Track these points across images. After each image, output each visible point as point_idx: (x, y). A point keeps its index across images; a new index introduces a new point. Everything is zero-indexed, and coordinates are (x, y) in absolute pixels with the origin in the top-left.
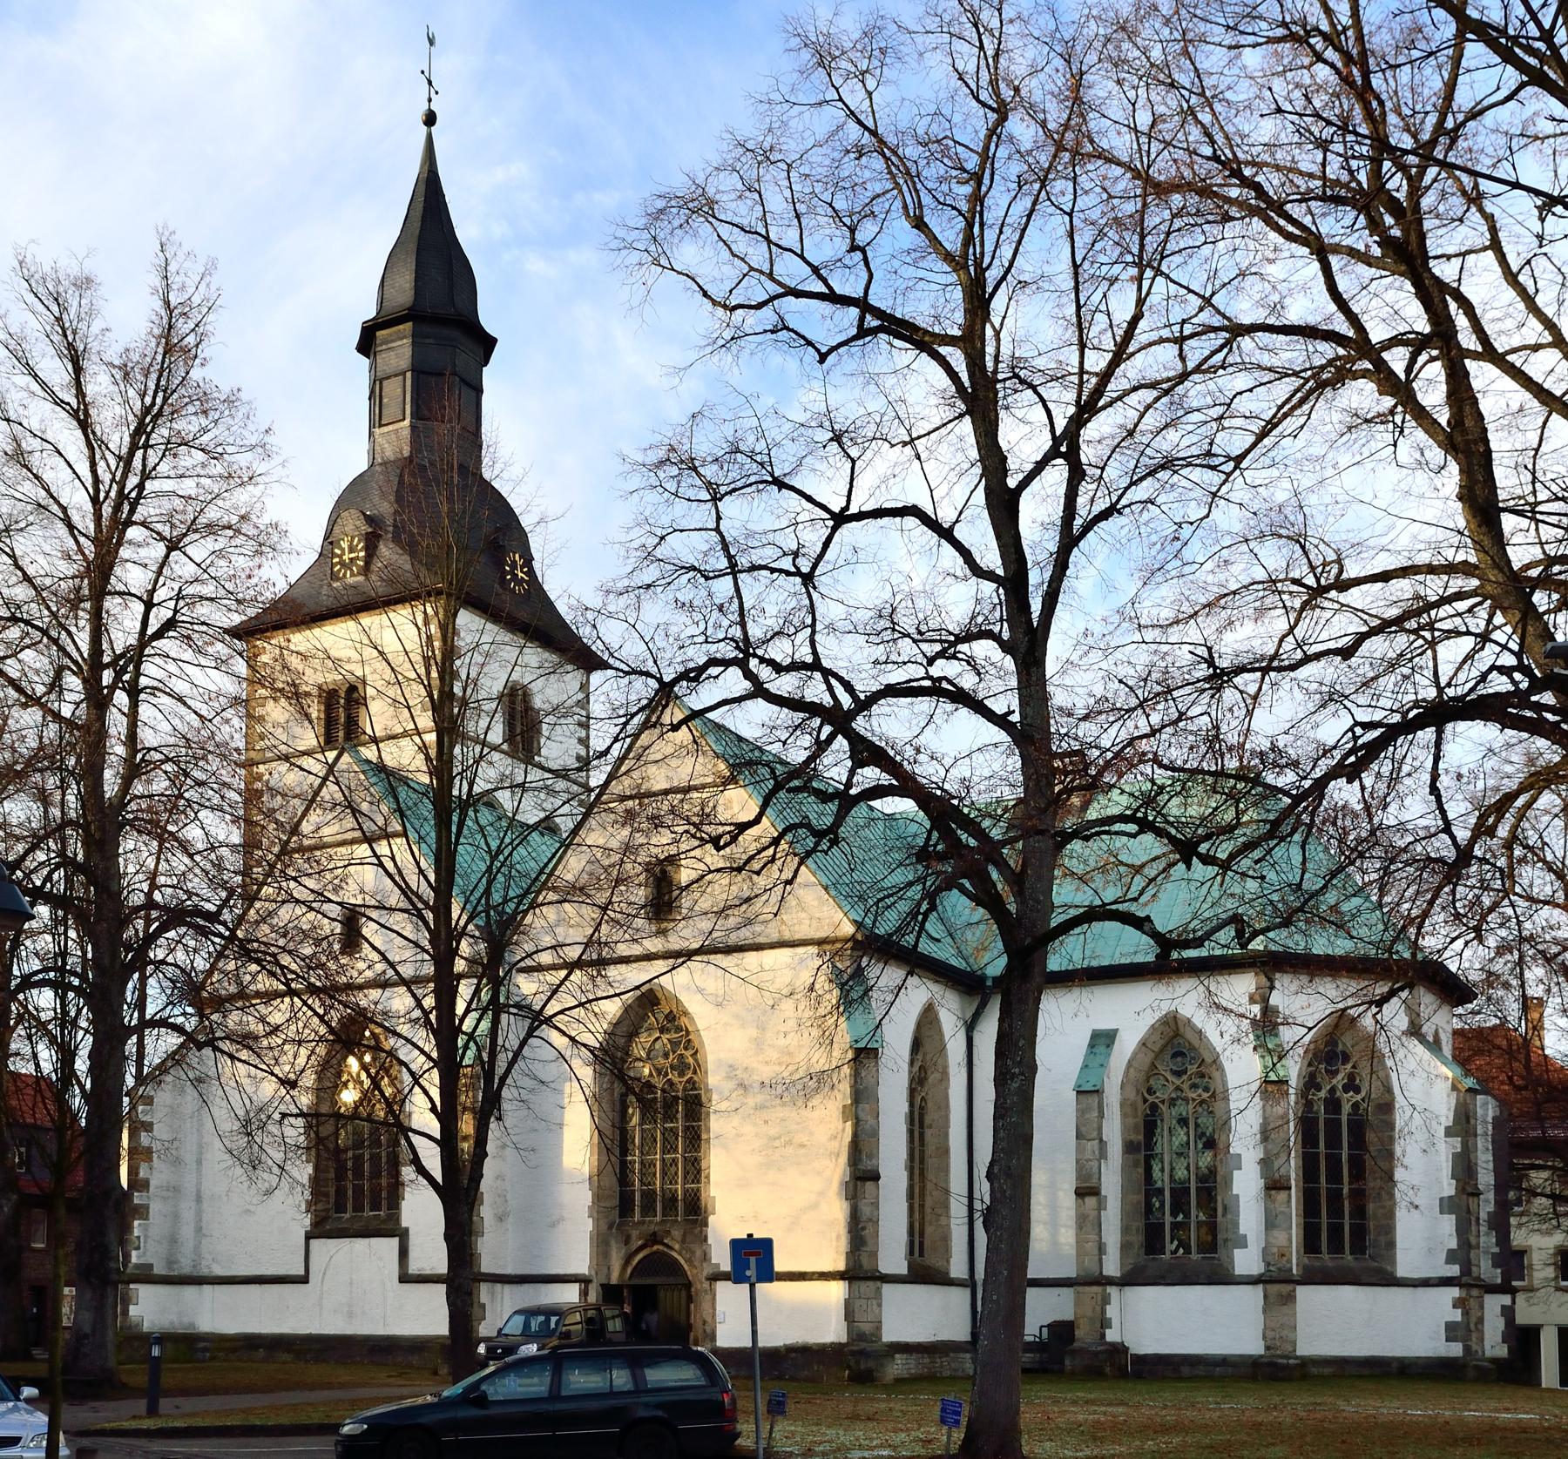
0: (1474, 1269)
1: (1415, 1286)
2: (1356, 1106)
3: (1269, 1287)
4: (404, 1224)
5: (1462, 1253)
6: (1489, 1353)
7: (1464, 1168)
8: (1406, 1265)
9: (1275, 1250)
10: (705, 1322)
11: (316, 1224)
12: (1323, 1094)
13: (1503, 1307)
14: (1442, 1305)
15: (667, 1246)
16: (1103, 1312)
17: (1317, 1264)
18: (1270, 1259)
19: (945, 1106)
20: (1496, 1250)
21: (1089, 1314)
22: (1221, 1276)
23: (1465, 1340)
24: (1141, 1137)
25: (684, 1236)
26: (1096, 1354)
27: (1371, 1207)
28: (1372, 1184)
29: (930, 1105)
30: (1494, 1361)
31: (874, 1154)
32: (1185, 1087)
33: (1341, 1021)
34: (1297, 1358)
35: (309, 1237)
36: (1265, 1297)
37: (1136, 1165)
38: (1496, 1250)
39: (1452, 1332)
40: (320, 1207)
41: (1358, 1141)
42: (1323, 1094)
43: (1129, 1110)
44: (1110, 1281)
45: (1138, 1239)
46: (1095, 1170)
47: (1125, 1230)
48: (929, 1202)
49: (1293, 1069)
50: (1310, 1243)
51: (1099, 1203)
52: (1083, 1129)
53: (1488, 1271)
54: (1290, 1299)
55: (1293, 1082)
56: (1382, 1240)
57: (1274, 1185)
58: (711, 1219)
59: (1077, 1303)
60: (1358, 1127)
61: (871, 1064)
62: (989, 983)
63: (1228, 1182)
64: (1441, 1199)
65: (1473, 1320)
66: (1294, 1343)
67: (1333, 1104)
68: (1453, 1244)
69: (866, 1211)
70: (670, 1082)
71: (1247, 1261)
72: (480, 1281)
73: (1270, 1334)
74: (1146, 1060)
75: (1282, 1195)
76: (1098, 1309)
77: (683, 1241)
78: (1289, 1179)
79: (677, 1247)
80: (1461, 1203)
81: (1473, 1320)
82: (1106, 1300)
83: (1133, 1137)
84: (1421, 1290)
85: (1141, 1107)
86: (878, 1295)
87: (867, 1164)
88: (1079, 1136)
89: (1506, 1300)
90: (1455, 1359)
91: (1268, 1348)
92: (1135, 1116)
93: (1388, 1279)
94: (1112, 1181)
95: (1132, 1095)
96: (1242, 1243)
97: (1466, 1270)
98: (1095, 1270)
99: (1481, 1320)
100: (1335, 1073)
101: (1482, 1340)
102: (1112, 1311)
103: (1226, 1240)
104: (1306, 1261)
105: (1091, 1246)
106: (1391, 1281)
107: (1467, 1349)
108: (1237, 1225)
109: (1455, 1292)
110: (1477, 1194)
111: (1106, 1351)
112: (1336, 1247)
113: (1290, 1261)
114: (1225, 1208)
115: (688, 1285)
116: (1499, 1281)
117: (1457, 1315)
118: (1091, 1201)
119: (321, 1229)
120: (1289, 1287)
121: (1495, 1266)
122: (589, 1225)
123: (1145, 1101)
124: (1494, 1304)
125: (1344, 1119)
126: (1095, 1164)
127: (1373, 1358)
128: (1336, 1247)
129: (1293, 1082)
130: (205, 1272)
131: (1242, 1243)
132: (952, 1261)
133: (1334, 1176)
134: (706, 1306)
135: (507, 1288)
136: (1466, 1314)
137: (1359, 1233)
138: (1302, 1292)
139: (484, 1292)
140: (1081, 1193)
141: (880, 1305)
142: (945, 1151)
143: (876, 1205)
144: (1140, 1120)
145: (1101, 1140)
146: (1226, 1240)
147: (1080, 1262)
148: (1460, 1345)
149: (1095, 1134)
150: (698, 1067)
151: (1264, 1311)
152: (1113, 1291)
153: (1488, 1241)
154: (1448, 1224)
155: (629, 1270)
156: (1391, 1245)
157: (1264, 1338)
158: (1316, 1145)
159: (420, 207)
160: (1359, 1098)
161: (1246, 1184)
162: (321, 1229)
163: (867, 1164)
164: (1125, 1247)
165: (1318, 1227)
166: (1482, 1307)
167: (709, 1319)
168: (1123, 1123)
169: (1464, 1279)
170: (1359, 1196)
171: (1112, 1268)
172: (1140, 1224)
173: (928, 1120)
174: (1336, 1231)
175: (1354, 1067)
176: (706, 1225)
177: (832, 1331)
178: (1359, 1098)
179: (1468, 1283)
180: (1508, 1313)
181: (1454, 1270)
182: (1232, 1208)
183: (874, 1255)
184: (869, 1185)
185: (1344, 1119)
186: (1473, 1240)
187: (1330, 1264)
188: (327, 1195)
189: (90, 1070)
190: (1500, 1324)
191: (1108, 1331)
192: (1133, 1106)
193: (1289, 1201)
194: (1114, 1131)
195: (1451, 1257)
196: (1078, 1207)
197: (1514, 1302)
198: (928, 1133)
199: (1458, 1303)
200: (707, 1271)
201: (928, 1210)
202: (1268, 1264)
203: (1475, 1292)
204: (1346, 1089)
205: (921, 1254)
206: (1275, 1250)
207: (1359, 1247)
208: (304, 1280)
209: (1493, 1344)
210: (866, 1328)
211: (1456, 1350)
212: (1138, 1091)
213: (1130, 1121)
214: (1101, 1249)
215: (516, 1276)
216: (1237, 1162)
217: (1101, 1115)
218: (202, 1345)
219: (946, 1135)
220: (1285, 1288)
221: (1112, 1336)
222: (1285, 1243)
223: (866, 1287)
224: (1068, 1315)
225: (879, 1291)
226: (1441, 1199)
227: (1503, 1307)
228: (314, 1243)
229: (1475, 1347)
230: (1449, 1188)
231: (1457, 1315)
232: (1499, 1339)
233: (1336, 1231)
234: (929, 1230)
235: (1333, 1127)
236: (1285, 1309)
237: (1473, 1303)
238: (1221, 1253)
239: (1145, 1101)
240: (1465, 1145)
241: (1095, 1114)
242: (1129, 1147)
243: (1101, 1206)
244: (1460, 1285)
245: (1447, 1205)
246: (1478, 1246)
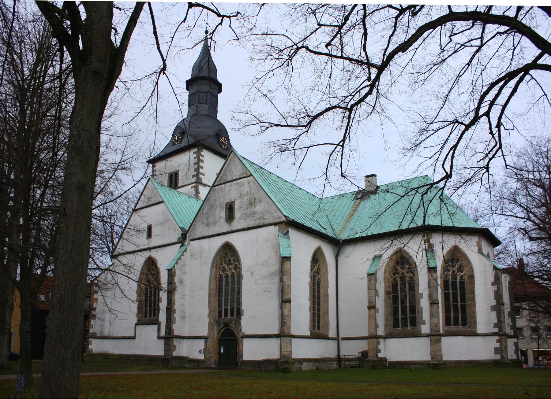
0: (503, 329)
1: (484, 336)
2: (462, 277)
3: (432, 337)
4: (160, 321)
5: (499, 324)
6: (510, 358)
7: (498, 296)
8: (481, 329)
9: (434, 324)
10: (240, 352)
11: (138, 321)
12: (450, 273)
13: (515, 343)
14: (493, 342)
15: (230, 326)
16: (377, 347)
17: (450, 329)
18: (432, 327)
19: (327, 281)
20: (511, 324)
21: (373, 348)
22: (417, 335)
23: (501, 354)
24: (391, 290)
25: (235, 323)
26: (374, 361)
27: (468, 310)
28: (468, 303)
29: (322, 281)
30: (512, 360)
31: (289, 293)
32: (405, 272)
33: (456, 250)
34: (443, 361)
35: (136, 325)
36: (431, 341)
37: (390, 299)
38: (511, 324)
39: (497, 351)
40: (140, 315)
41: (463, 288)
42: (450, 273)
43: (387, 281)
44: (380, 337)
45: (391, 323)
46: (374, 299)
47: (386, 320)
48: (321, 312)
49: (439, 263)
50: (447, 322)
51: (376, 311)
52: (370, 286)
53: (508, 330)
54: (440, 341)
55: (439, 269)
56: (472, 320)
57: (433, 303)
58: (242, 317)
59: (369, 344)
60: (462, 283)
61: (288, 262)
62: (341, 241)
63: (419, 303)
64: (491, 306)
65: (504, 346)
66: (441, 356)
67: (454, 276)
68: (496, 321)
69: (286, 312)
70: (233, 273)
71: (425, 329)
72: (173, 338)
73: (432, 353)
74: (392, 264)
75: (435, 306)
76: (375, 346)
77: (235, 325)
78: (438, 300)
79: (233, 327)
80: (498, 307)
81: (504, 346)
82: (379, 343)
83: (389, 290)
84: (485, 337)
85: (391, 280)
86: (290, 342)
87: (286, 297)
88: (369, 289)
89: (515, 340)
90: (498, 360)
91: (432, 358)
92: (389, 282)
93: (475, 334)
94: (381, 303)
95: (387, 275)
96: (424, 323)
97: (501, 330)
98: (374, 333)
99: (506, 347)
100: (453, 266)
101: (507, 353)
102: (380, 347)
103: (419, 322)
104: (446, 328)
105: (373, 326)
106: (475, 334)
107: (502, 357)
108: (422, 317)
109: (497, 338)
110: (503, 304)
111: (377, 361)
112: (405, 325)
113: (439, 328)
114: (418, 311)
115: (237, 339)
116: (513, 334)
117: (498, 345)
118: (373, 310)
119: (140, 323)
120: (439, 337)
121: (511, 329)
122: (208, 320)
123: (392, 277)
124: (511, 343)
125: (458, 281)
126: (374, 298)
127: (470, 360)
128: (405, 325)
129: (439, 269)
130: (111, 335)
131: (424, 323)
132: (330, 331)
133: (455, 300)
134: (241, 346)
135: (185, 340)
136: (501, 345)
137: (220, 280)
138: (444, 339)
139: (175, 342)
140: (369, 308)
141: (291, 345)
142: (327, 296)
143: (290, 311)
144: (391, 284)
145: (376, 290)
146: (419, 322)
147: (369, 331)
148: (499, 355)
149: (373, 288)
150: (240, 269)
151: (431, 346)
152: (381, 340)
153: (508, 321)
154: (494, 315)
155: (220, 334)
156: (475, 322)
157: (431, 354)
158: (449, 290)
159: (203, 51)
160: (463, 274)
161: (424, 303)
162: (140, 323)
163: (286, 297)
164: (386, 325)
165: (450, 317)
166: (506, 342)
167: (241, 351)
168: (385, 285)
169: (501, 333)
170: (464, 308)
171: (381, 331)
172: (391, 318)
173: (321, 286)
174: (456, 318)
175: (461, 264)
176: (241, 319)
177: (276, 356)
178: (463, 274)
179: (501, 335)
180: (516, 344)
181: (497, 330)
182: (421, 311)
183: (289, 328)
184: (287, 304)
185: (458, 281)
186: (502, 319)
187: (454, 329)
188: (142, 312)
189: (20, 273)
190: (514, 348)
191: (379, 354)
192: (388, 279)
193: (438, 307)
194: (381, 287)
195: (495, 326)
196: (369, 312)
197: (518, 341)
198: (321, 290)
199: (498, 341)
200: (241, 335)
201: (321, 315)
202: (431, 329)
203: (504, 337)
204: (458, 271)
205: (319, 329)
206: (434, 324)
207: (464, 324)
208: (134, 338)
209: (511, 355)
210: (286, 353)
211: (498, 357)
212: (390, 275)
213: (387, 284)
214: (377, 326)
215: (188, 337)
216: (421, 296)
217: (376, 281)
218: (109, 357)
219: (327, 291)
220: (438, 338)
221: (380, 355)
222: (437, 322)
223: (286, 340)
224: (366, 349)
225: (291, 340)
226: (491, 306)
227: (515, 343)
228: (137, 327)
229: (504, 356)
230: (494, 302)
231: (498, 345)
232: (513, 353)
233: (456, 318)
234: (321, 321)
235: (454, 283)
236: (437, 345)
237: (503, 341)
238: (418, 326)
239: (392, 277)
240: (498, 288)
241: (374, 281)
242: (387, 293)
243: (376, 311)
244: (499, 335)
245: (493, 308)
246: (504, 322)
